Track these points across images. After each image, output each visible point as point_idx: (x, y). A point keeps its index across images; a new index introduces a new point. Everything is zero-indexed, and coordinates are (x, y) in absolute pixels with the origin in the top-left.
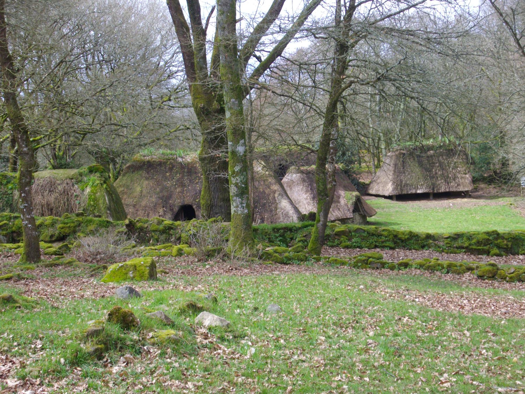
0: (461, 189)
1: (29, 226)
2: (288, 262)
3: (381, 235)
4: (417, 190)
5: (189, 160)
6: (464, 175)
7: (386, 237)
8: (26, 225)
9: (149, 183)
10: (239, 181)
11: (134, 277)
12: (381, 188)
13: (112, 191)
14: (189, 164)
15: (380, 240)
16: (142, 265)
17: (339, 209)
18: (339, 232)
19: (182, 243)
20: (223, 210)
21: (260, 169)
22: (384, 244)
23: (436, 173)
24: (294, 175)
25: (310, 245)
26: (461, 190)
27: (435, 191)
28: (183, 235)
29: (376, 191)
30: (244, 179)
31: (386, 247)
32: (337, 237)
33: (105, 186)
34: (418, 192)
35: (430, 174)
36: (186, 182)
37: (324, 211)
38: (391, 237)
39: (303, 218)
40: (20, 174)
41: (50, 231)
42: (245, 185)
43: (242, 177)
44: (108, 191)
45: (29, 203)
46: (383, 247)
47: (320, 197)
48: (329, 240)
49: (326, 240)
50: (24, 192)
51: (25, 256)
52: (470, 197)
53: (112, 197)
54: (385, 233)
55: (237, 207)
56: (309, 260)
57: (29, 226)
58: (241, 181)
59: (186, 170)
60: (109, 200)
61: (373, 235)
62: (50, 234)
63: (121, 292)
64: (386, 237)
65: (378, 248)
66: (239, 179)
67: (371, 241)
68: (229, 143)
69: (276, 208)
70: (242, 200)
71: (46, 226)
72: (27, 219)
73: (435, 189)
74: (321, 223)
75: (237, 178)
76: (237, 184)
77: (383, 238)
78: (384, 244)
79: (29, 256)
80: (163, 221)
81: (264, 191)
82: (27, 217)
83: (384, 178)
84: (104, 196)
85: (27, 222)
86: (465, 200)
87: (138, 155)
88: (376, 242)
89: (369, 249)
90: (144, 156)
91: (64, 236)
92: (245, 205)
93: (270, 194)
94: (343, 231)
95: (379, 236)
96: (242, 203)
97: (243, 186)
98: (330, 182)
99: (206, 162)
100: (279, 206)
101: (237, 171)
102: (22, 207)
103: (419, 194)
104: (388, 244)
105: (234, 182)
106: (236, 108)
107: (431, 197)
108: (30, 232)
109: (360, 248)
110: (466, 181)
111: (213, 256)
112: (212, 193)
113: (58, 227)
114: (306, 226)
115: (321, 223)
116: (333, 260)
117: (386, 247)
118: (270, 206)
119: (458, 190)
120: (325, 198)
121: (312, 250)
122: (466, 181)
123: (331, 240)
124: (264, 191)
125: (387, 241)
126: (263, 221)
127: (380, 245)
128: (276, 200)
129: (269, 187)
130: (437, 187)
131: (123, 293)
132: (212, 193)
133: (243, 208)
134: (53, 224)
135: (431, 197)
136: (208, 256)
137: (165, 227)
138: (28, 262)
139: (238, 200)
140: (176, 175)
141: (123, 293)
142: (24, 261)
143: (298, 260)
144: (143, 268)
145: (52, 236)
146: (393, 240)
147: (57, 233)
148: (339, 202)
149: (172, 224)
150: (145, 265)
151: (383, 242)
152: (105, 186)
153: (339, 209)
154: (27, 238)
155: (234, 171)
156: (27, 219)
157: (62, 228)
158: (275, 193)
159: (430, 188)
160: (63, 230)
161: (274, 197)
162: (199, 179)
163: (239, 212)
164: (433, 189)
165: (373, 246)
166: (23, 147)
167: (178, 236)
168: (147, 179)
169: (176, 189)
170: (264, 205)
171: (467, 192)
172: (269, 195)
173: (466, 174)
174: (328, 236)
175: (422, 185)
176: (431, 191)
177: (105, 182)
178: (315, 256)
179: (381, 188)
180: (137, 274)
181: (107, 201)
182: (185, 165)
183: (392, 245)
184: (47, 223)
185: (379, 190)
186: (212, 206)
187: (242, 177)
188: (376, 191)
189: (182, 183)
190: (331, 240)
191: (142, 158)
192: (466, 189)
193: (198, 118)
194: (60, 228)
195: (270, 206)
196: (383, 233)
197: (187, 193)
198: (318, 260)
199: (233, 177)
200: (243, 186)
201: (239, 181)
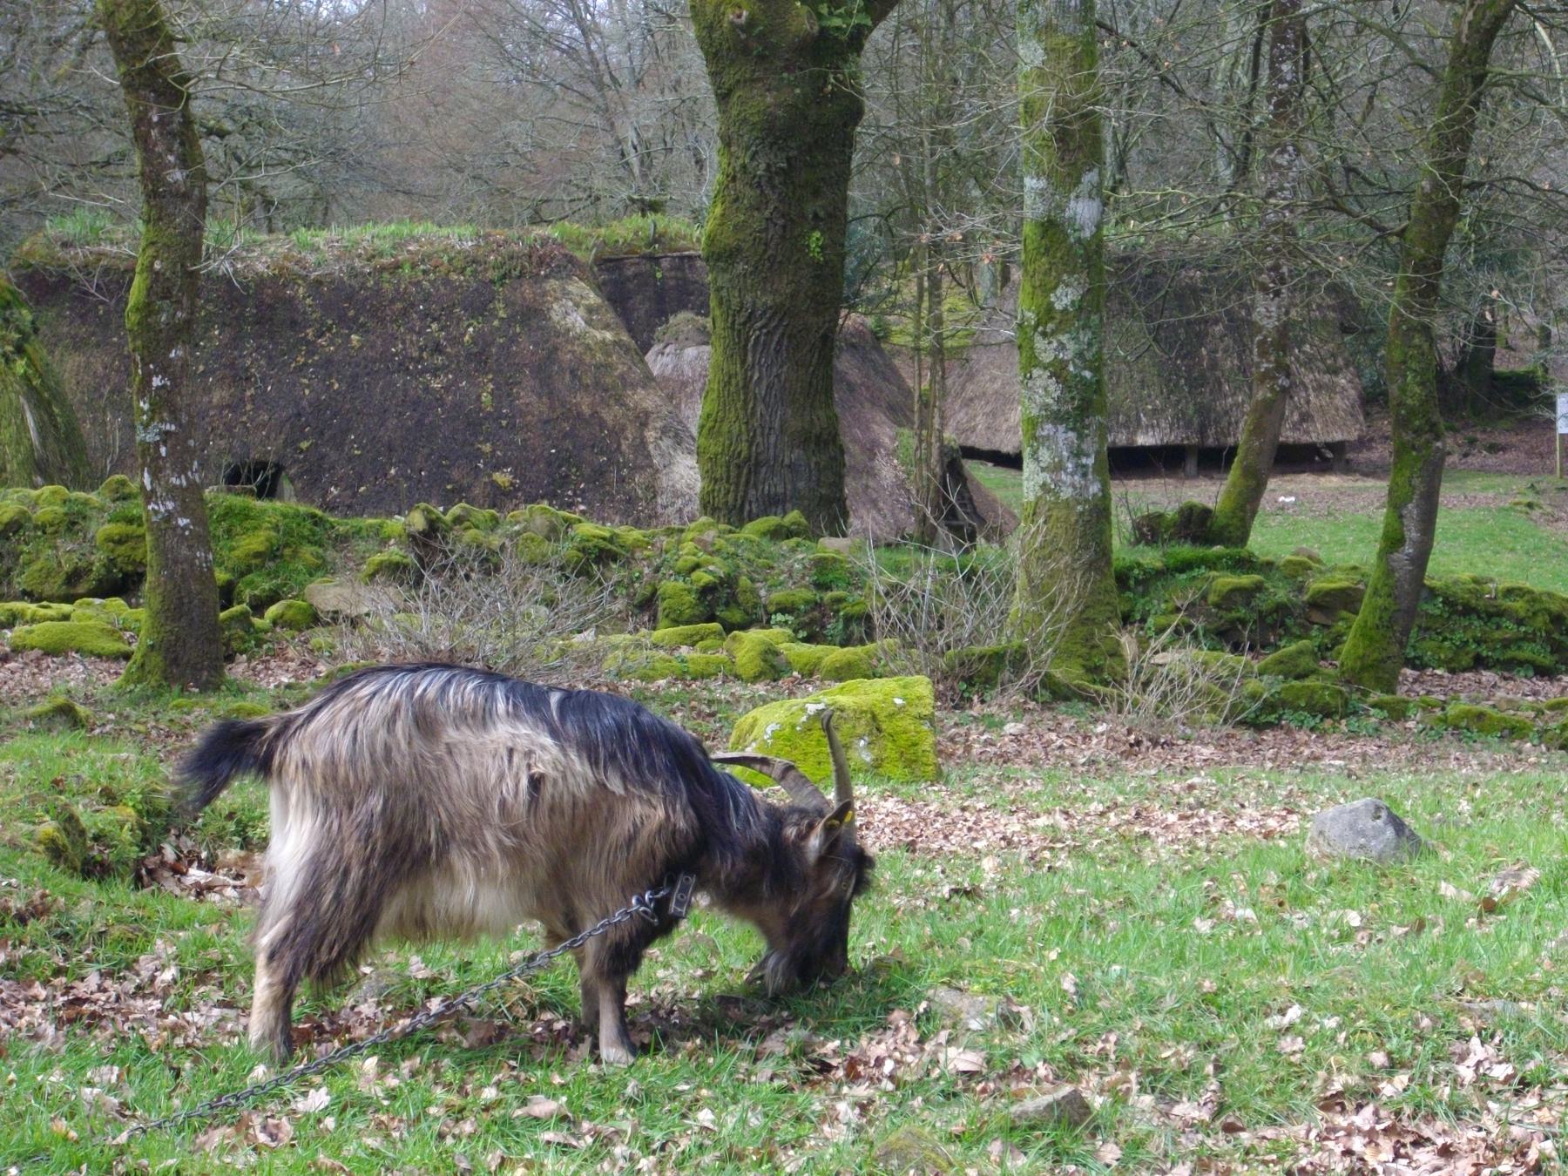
0: (1317, 434)
1: (182, 522)
2: (1263, 719)
3: (1501, 613)
4: (1134, 433)
5: (260, 268)
6: (1326, 378)
7: (1520, 622)
8: (169, 517)
9: (88, 364)
10: (1068, 355)
11: (878, 764)
12: (981, 422)
13: (49, 389)
14: (261, 281)
15: (1497, 635)
16: (901, 709)
17: (874, 503)
18: (1329, 593)
19: (662, 621)
20: (801, 485)
21: (577, 320)
22: (1512, 653)
23: (1214, 365)
24: (691, 352)
25: (1349, 648)
26: (1314, 438)
27: (1211, 442)
28: (670, 586)
29: (960, 431)
30: (1090, 344)
31: (1521, 663)
32: (1316, 616)
33: (20, 366)
34: (1142, 440)
35: (1189, 370)
36: (251, 359)
37: (1422, 496)
38: (1540, 621)
39: (1152, 529)
40: (150, 289)
41: (67, 553)
42: (1096, 371)
43: (1085, 337)
44: (32, 389)
45: (184, 419)
46: (1508, 666)
47: (1408, 437)
48: (1287, 630)
49: (1273, 627)
50: (163, 371)
51: (156, 659)
52: (1348, 468)
53: (51, 415)
54: (1519, 605)
55: (1057, 467)
56: (1355, 713)
57: (182, 522)
58: (1080, 355)
59: (250, 311)
60: (41, 430)
61: (1468, 611)
62: (67, 568)
63: (1352, 826)
64: (1520, 622)
65: (1487, 668)
66: (1072, 347)
67: (1459, 636)
68: (1029, 182)
69: (652, 491)
70: (1081, 437)
71: (42, 528)
72: (173, 492)
73: (1211, 432)
74: (1409, 549)
75: (1064, 338)
76: (1063, 365)
77: (1510, 629)
78: (1512, 653)
79: (175, 662)
80: (569, 523)
81: (595, 414)
82: (174, 480)
83: (993, 379)
84: (20, 411)
85: (170, 505)
86: (1332, 481)
87: (40, 238)
88: (1478, 642)
89: (1452, 671)
90: (65, 245)
91: (126, 575)
92: (1090, 461)
93: (623, 429)
94: (1343, 591)
95: (1490, 616)
96: (1078, 454)
97: (1087, 374)
98: (1266, 376)
99: (741, 267)
100: (664, 481)
101: (1065, 311)
102: (151, 437)
103: (1143, 448)
104: (1527, 652)
105: (1047, 358)
106: (1069, 25)
107: (1191, 465)
108: (184, 551)
109: (1414, 668)
110: (1338, 400)
111: (989, 682)
112: (760, 408)
113: (100, 536)
114: (1186, 566)
115: (1409, 549)
116: (1466, 715)
117: (1521, 663)
118: (622, 480)
119: (1305, 439)
120: (1428, 442)
121: (1363, 669)
122: (1338, 400)
123: (1296, 630)
124: (595, 414)
125: (1525, 638)
126: (703, 545)
127: (1497, 655)
128: (648, 456)
129: (620, 401)
130: (1217, 422)
131: (1362, 833)
132: (760, 408)
133: (1084, 475)
134: (73, 523)
135: (1191, 465)
136: (970, 681)
137: (583, 550)
138: (176, 689)
139: (1061, 436)
140: (207, 330)
141: (1362, 833)
142: (153, 681)
143: (1312, 709)
144: (906, 723)
145: (74, 577)
146: (1549, 638)
147: (98, 559)
148: (872, 473)
149: (611, 540)
150: (914, 711)
151: (1506, 643)
152: (20, 366)
153: (874, 503)
154: (171, 577)
155: (1050, 308)
156: (173, 492)
157: (120, 541)
158: (644, 425)
159: (1188, 425)
160: (121, 549)
161: (643, 443)
162: (310, 354)
163: (1066, 493)
164: (1202, 431)
165: (1466, 660)
166: (168, 166)
167: (641, 590)
168: (78, 345)
169: (208, 390)
170: (600, 473)
171: (1338, 447)
172: (617, 432)
173: (1335, 371)
174: (1282, 609)
175: (1155, 411)
176: (1195, 440)
177: (20, 350)
178: (1376, 696)
179: (981, 422)
180: (890, 752)
181: (33, 434)
182: (246, 287)
183: (1547, 660)
184: (43, 513)
185: (973, 430)
186: (758, 464)
187: (1085, 337)
188: (960, 431)
189: (232, 365)
190: (1296, 630)
191: (60, 253)
192: (1338, 436)
193: (713, 74)
194: (109, 539)
195: (622, 480)
196: (1508, 603)
197: (256, 409)
198: (1397, 713)
199: (1044, 334)
200: (1087, 374)
201: (1068, 355)
